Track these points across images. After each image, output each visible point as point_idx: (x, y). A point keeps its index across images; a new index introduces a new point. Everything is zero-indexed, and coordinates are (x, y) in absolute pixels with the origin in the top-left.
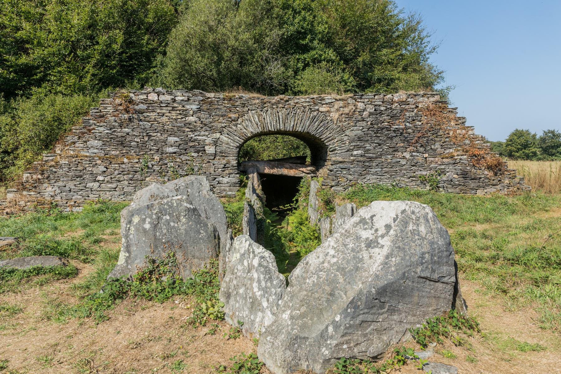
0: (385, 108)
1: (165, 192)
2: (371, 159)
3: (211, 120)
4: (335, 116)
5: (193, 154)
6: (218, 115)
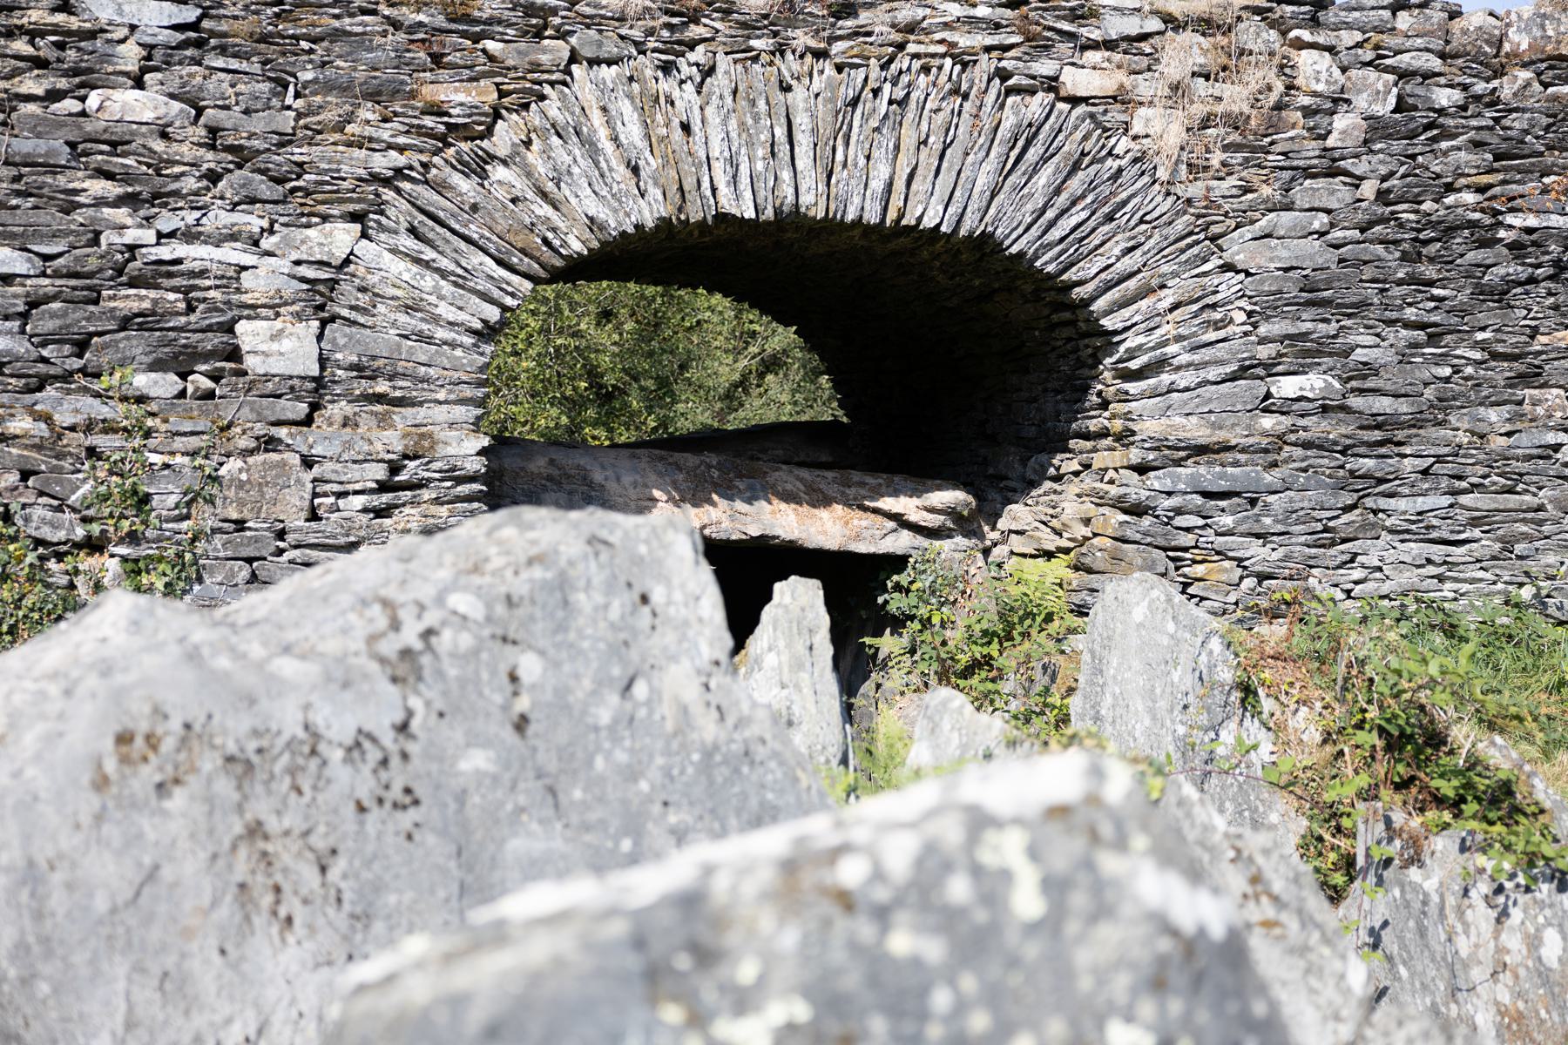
0: (1457, 96)
1: (277, 686)
2: (1387, 433)
3: (286, 121)
4: (1161, 128)
5: (142, 381)
6: (345, 89)
